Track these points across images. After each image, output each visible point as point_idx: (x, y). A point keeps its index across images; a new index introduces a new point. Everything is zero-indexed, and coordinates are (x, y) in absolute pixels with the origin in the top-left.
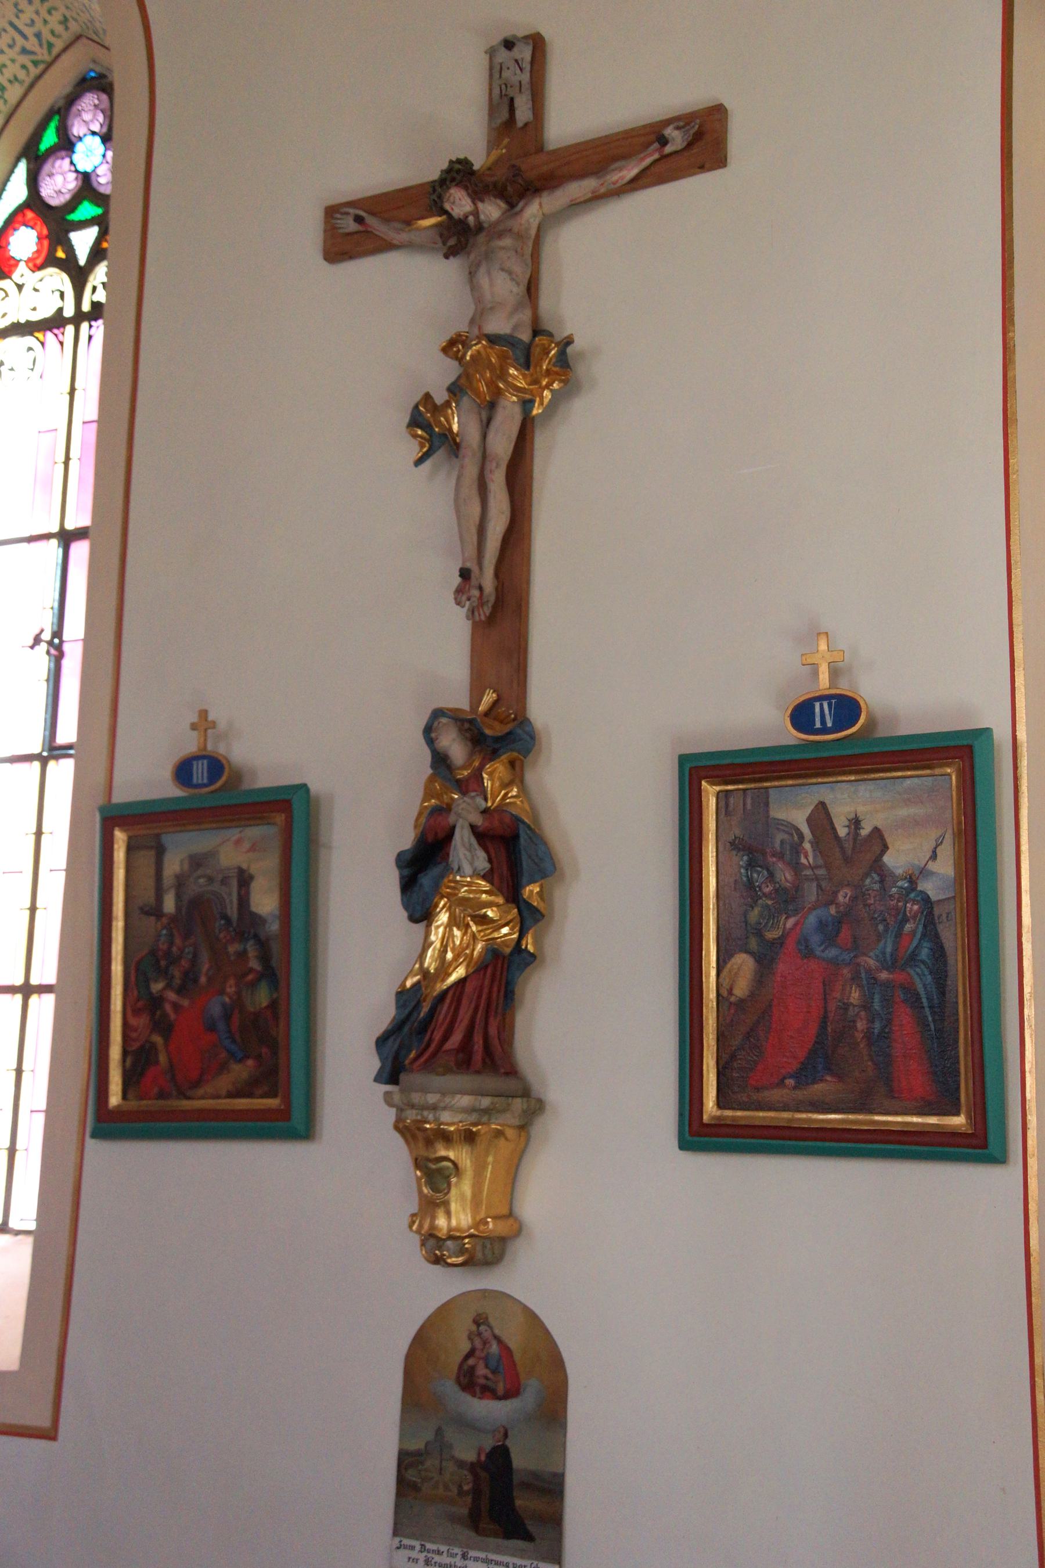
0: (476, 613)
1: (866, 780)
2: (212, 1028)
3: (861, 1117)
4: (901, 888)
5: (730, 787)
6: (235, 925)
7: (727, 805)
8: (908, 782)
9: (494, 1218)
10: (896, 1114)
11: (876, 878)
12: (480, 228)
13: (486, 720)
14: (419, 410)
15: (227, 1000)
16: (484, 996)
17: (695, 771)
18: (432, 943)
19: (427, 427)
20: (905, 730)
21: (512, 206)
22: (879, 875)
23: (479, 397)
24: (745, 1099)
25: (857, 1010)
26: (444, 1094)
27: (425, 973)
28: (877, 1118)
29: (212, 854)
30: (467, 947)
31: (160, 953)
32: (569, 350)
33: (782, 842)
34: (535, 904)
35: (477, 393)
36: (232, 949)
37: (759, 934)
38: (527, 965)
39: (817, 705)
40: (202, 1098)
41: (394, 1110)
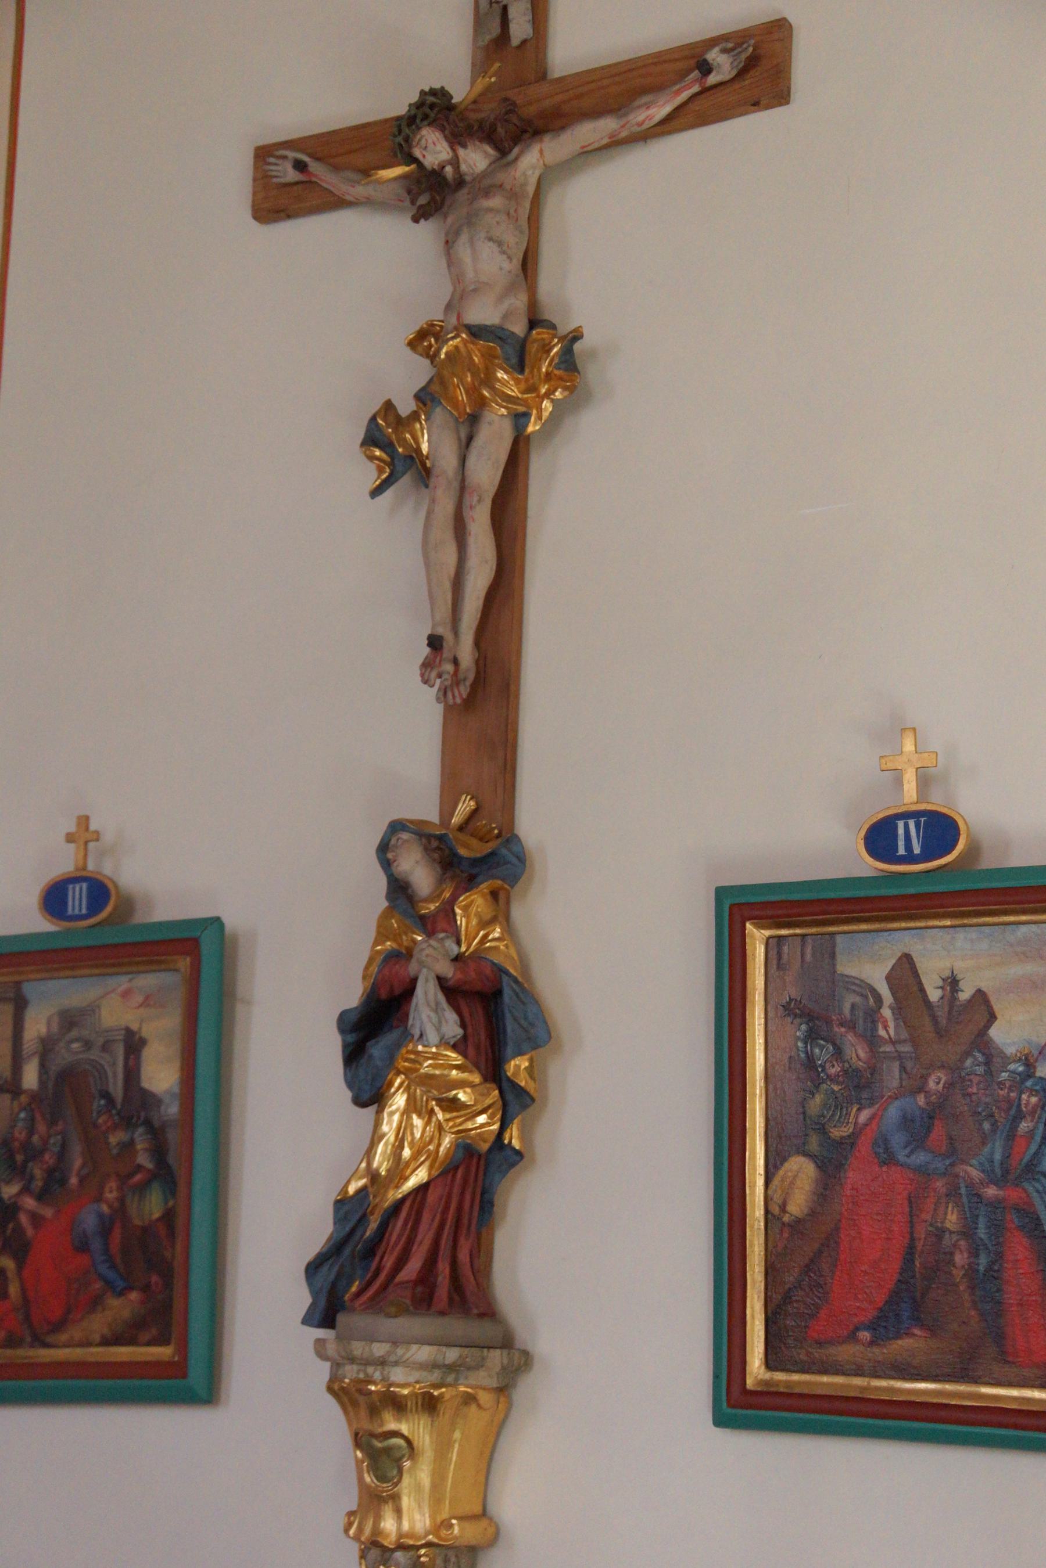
0: (450, 695)
1: (964, 926)
2: (83, 1247)
3: (962, 1388)
4: (1013, 1072)
5: (784, 932)
6: (119, 1107)
7: (779, 954)
8: (1024, 929)
9: (460, 1518)
10: (1010, 1385)
11: (980, 1058)
12: (460, 182)
13: (460, 835)
14: (377, 425)
15: (105, 1208)
16: (453, 1206)
17: (738, 910)
18: (384, 1135)
19: (387, 446)
20: (1017, 860)
21: (503, 152)
22: (984, 1054)
23: (457, 410)
24: (803, 1357)
25: (955, 1237)
26: (395, 1343)
27: (374, 1176)
28: (986, 1390)
29: (91, 1010)
30: (430, 1142)
31: (17, 1144)
32: (577, 347)
33: (853, 1006)
34: (523, 1084)
35: (455, 404)
36: (113, 1140)
37: (822, 1130)
38: (513, 1165)
39: (901, 824)
40: (66, 1346)
41: (328, 1364)
